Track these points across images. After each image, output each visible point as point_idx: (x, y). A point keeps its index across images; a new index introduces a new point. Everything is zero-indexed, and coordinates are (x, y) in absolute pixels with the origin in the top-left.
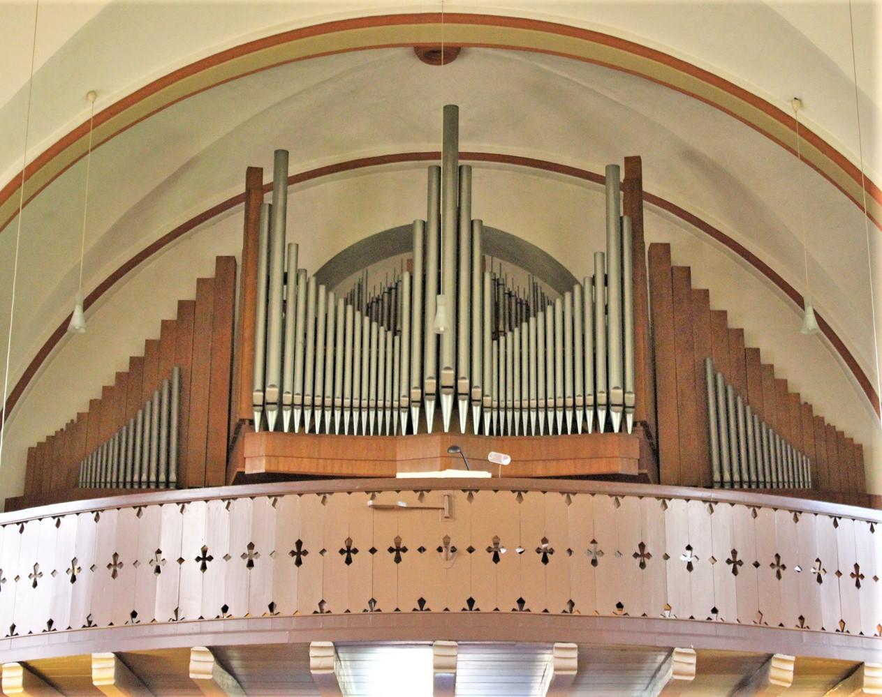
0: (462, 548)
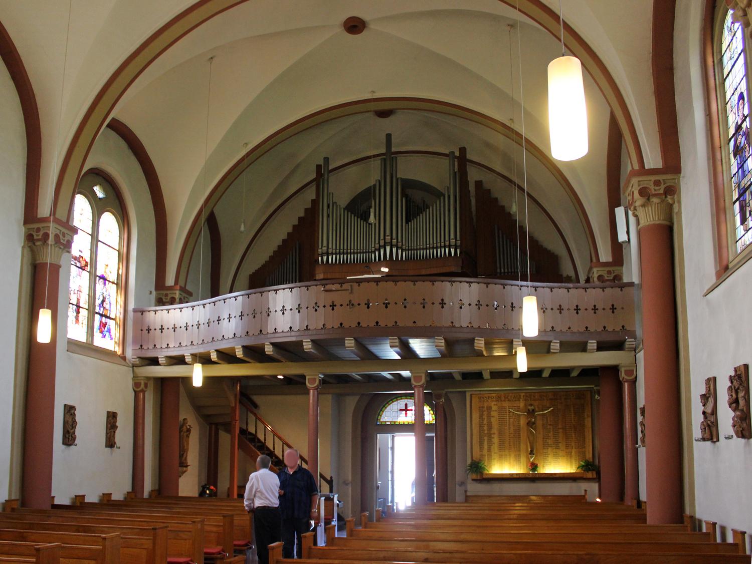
0: (356, 304)
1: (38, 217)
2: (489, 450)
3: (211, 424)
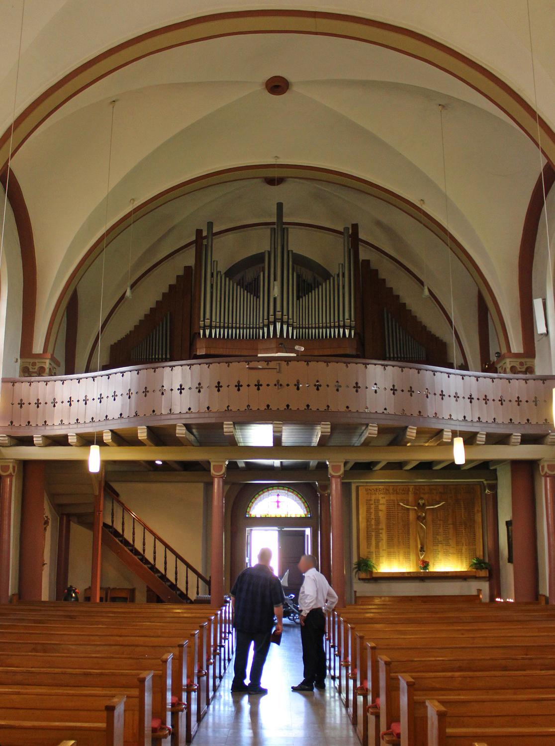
0: (284, 384)
2: (377, 547)
3: (62, 516)
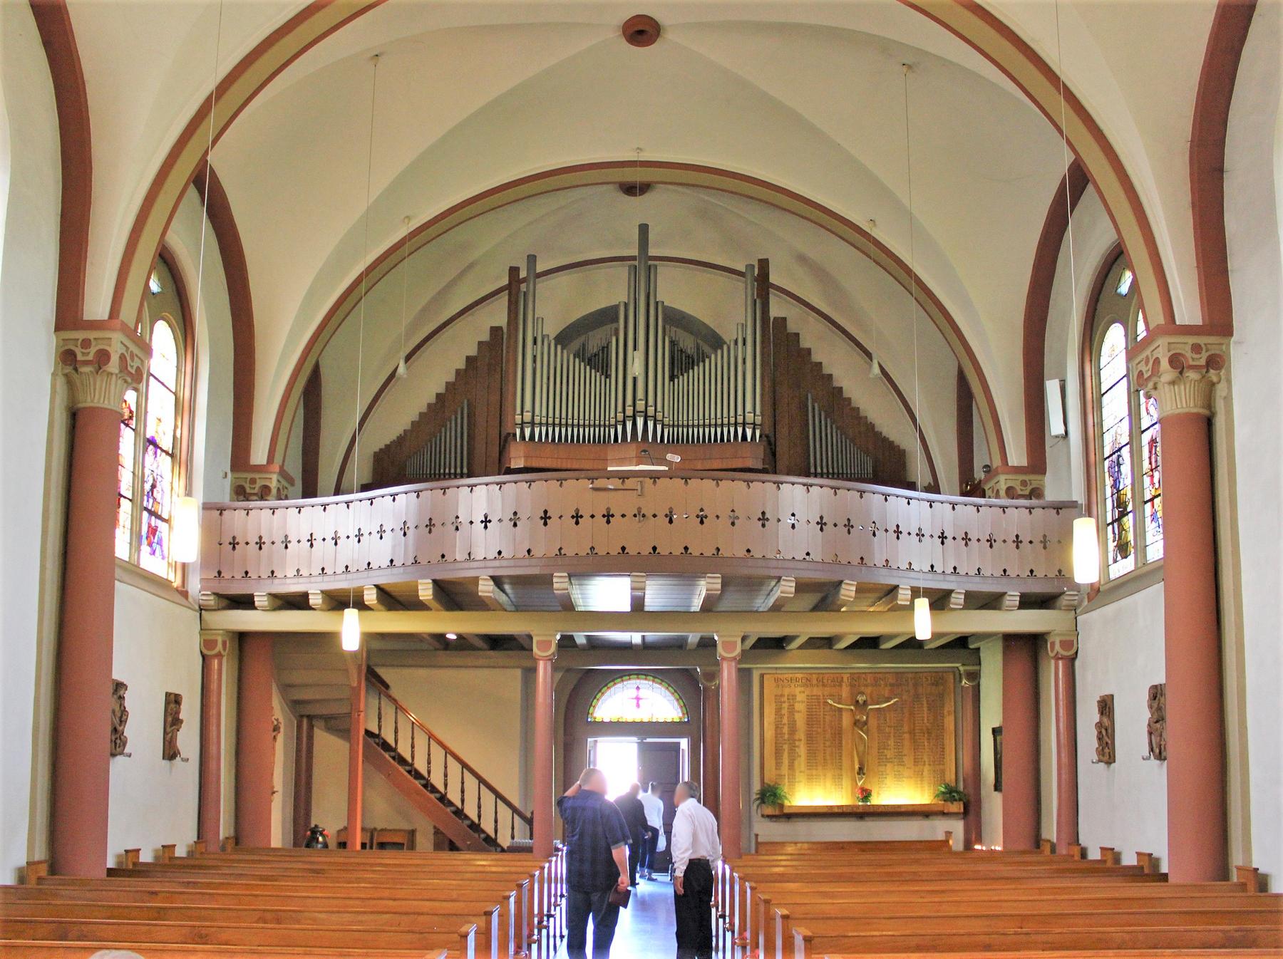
0: (649, 514)
1: (85, 318)
2: (791, 766)
